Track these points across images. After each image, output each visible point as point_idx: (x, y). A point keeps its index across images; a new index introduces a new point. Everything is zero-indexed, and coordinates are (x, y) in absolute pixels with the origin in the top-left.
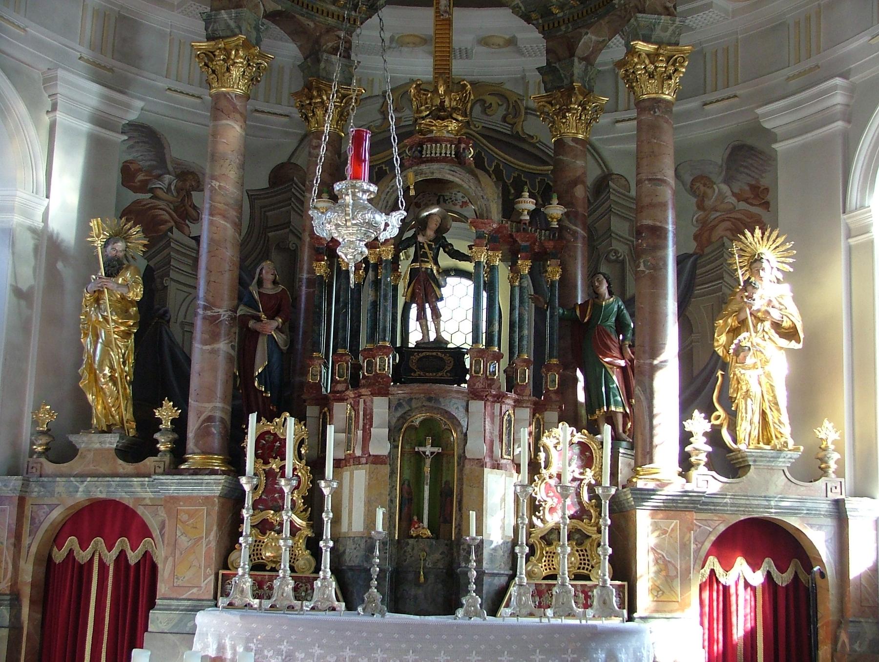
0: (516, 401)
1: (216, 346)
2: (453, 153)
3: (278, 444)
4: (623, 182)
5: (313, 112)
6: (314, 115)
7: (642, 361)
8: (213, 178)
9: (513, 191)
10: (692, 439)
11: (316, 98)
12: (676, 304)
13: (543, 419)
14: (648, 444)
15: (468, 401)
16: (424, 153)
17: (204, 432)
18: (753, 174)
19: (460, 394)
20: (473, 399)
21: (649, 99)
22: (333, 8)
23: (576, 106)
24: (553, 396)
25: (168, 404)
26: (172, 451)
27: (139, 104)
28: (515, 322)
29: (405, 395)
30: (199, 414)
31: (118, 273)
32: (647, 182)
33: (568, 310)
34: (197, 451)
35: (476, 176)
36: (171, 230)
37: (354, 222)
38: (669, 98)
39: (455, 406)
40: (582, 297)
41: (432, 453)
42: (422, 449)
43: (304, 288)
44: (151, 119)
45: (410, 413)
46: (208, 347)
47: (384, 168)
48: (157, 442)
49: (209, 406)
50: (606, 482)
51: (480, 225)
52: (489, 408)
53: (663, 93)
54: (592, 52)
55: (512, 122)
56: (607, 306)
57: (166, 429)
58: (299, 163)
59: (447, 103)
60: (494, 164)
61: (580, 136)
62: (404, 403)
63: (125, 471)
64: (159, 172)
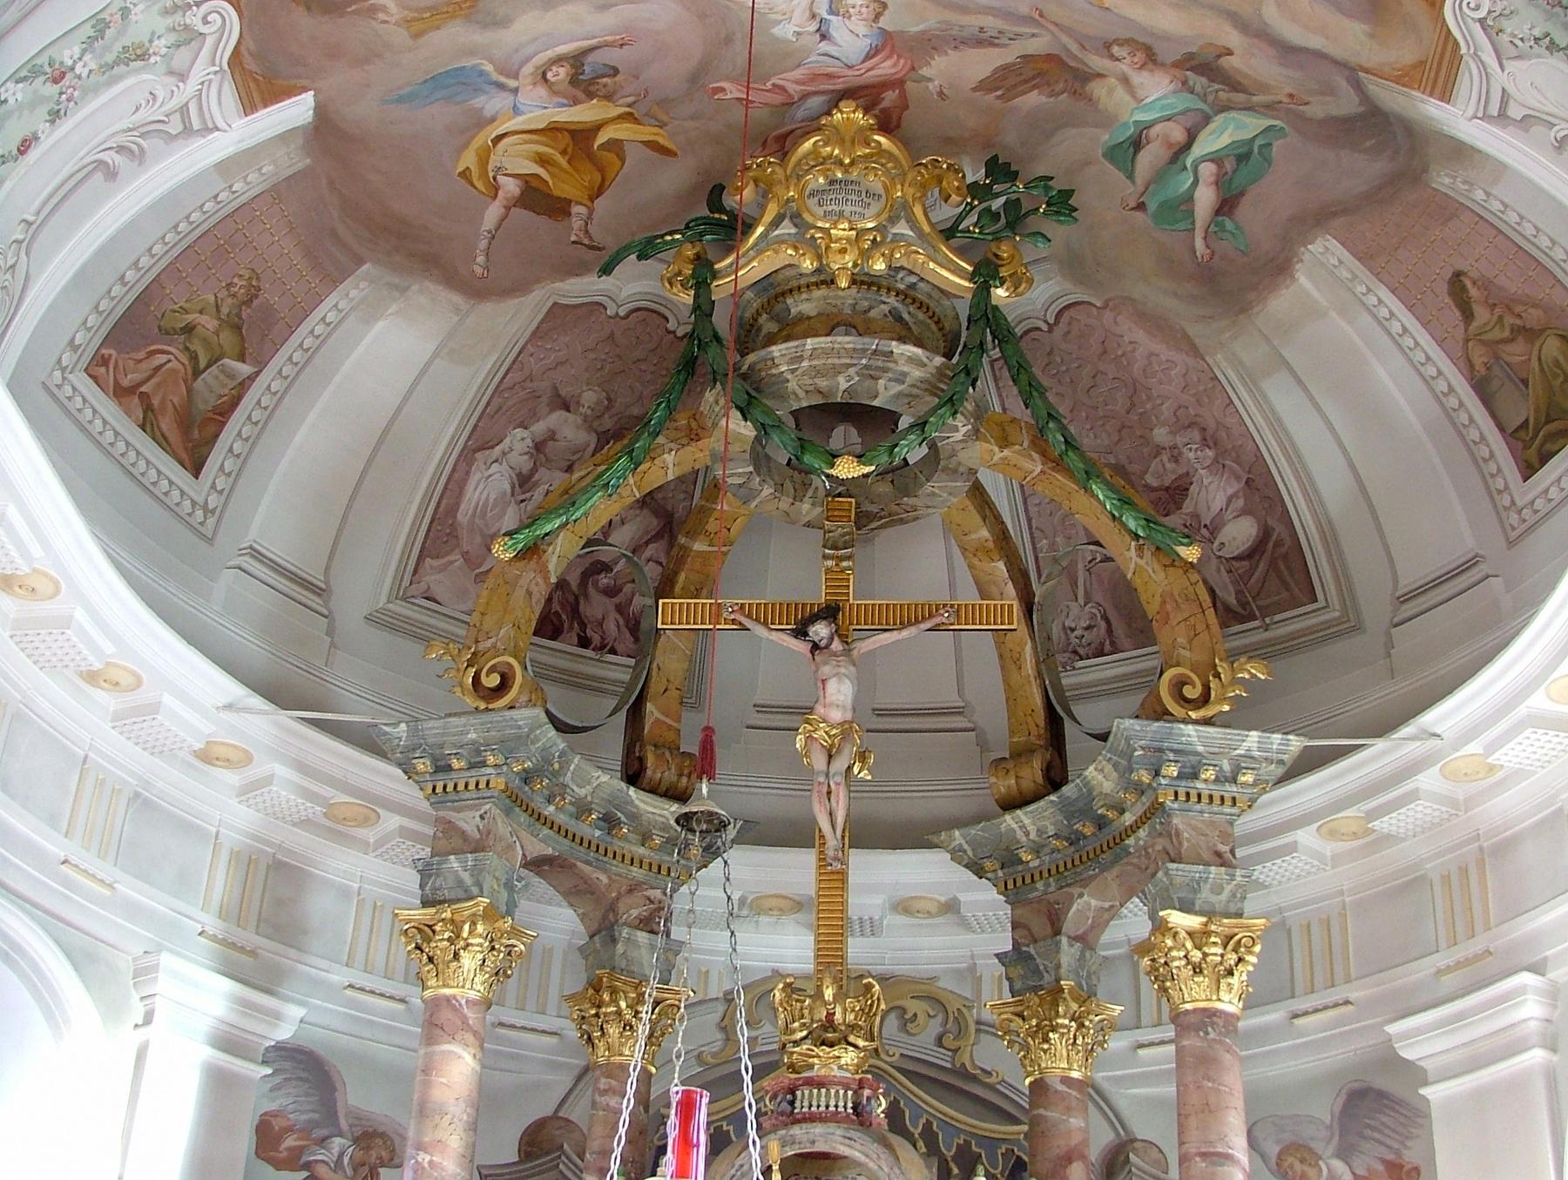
4: (1154, 1154)
8: (420, 1147)
9: (956, 1171)
11: (608, 1005)
16: (798, 1104)
18: (1389, 1142)
21: (1195, 1010)
22: (641, 850)
27: (297, 1012)
32: (1198, 1159)
35: (888, 1146)
44: (316, 1039)
47: (725, 1128)
54: (1092, 927)
59: (838, 1017)
64: (324, 1132)
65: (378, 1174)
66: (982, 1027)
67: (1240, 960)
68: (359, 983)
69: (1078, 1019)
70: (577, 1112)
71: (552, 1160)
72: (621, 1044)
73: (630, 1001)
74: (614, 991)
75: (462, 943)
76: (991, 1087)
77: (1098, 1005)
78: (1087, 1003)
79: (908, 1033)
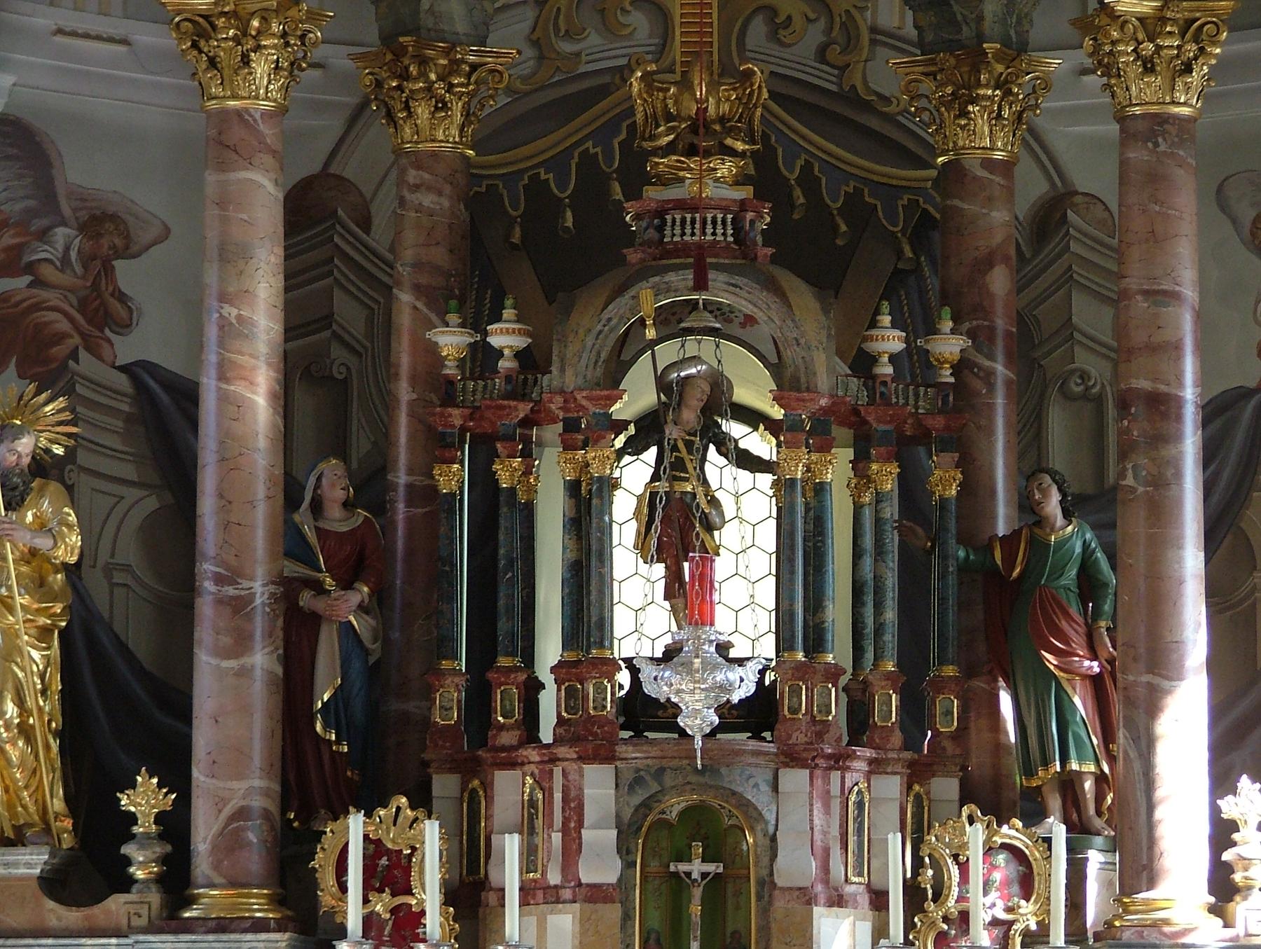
0: (871, 762)
1: (246, 660)
2: (730, 232)
3: (384, 861)
4: (1098, 211)
5: (407, 107)
6: (410, 115)
7: (1131, 678)
8: (224, 298)
9: (844, 228)
10: (1235, 836)
11: (416, 79)
12: (1202, 554)
13: (928, 793)
14: (1145, 849)
15: (777, 770)
16: (668, 232)
17: (229, 842)
19: (761, 758)
20: (786, 765)
21: (1143, 116)
23: (990, 92)
24: (947, 744)
25: (147, 783)
26: (160, 880)
28: (864, 584)
29: (649, 762)
30: (220, 803)
31: (23, 500)
32: (1139, 298)
33: (976, 550)
34: (218, 880)
36: (74, 355)
37: (702, 686)
38: (1185, 111)
39: (752, 782)
40: (1008, 519)
41: (704, 875)
42: (683, 867)
43: (401, 506)
45: (660, 797)
46: (226, 664)
47: (543, 177)
48: (128, 861)
49: (240, 786)
50: (1057, 938)
51: (794, 404)
52: (819, 782)
53: (1173, 103)
55: (841, 64)
56: (1061, 544)
57: (147, 835)
58: (348, 174)
59: (712, 110)
60: (800, 163)
61: (999, 155)
62: (648, 778)
63: (63, 924)
64: (45, 222)
65: (113, 267)
66: (879, 37)
67: (1202, 50)
68: (69, 25)
69: (1003, 84)
70: (350, 169)
71: (325, 231)
72: (433, 128)
73: (440, 70)
74: (423, 62)
75: (251, 44)
76: (889, 118)
77: (1029, 64)
78: (1015, 63)
79: (782, 44)
